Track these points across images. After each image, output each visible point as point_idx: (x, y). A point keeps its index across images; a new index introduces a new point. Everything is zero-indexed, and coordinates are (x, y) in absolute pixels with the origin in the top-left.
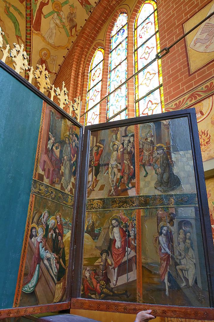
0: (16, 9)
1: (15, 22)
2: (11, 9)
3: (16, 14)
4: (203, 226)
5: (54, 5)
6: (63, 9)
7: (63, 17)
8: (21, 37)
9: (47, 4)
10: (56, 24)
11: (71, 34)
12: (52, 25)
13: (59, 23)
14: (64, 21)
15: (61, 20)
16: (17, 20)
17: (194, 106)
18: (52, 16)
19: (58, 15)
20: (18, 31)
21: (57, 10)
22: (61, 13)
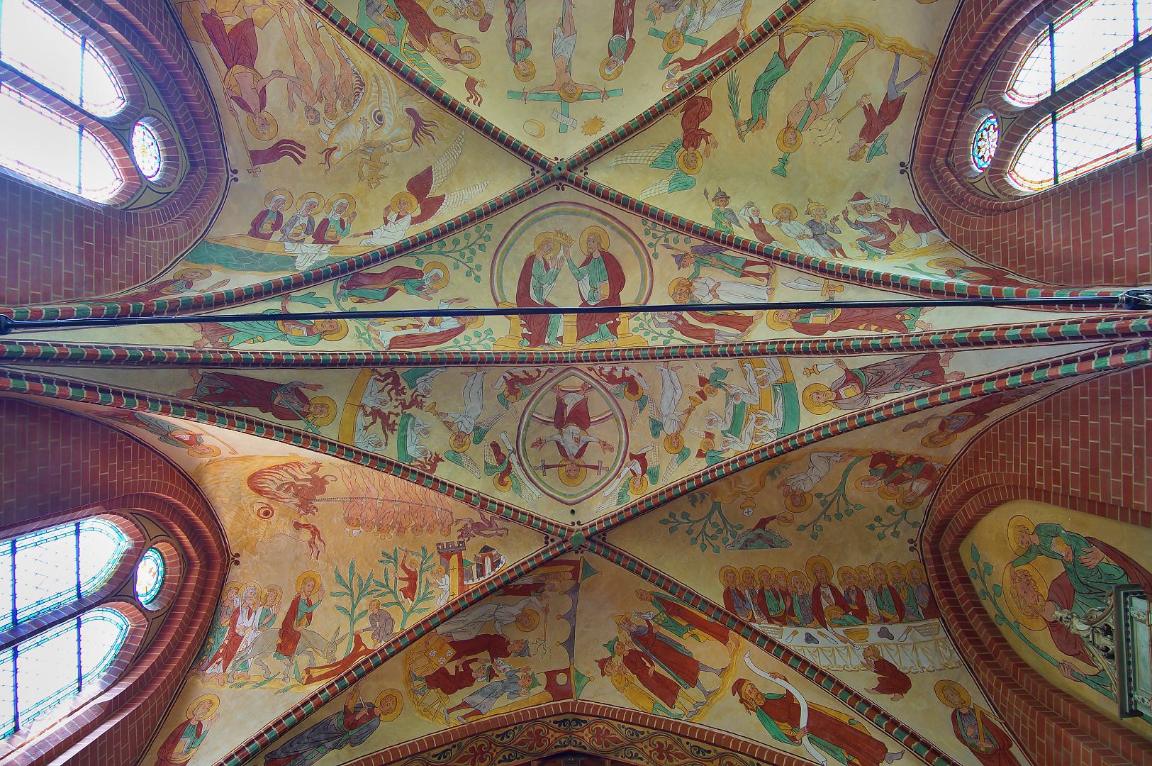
0: (734, 107)
1: (762, 93)
2: (745, 115)
3: (745, 98)
4: (58, 328)
5: (675, 49)
6: (669, 29)
7: (682, 16)
8: (781, 53)
9: (680, 60)
10: (704, 15)
11: (839, 388)
12: (711, 19)
13: (698, 12)
14: (687, 9)
15: (691, 15)
16: (755, 91)
17: (231, 287)
18: (695, 35)
19: (687, 28)
20: (773, 72)
21: (679, 37)
22: (679, 25)
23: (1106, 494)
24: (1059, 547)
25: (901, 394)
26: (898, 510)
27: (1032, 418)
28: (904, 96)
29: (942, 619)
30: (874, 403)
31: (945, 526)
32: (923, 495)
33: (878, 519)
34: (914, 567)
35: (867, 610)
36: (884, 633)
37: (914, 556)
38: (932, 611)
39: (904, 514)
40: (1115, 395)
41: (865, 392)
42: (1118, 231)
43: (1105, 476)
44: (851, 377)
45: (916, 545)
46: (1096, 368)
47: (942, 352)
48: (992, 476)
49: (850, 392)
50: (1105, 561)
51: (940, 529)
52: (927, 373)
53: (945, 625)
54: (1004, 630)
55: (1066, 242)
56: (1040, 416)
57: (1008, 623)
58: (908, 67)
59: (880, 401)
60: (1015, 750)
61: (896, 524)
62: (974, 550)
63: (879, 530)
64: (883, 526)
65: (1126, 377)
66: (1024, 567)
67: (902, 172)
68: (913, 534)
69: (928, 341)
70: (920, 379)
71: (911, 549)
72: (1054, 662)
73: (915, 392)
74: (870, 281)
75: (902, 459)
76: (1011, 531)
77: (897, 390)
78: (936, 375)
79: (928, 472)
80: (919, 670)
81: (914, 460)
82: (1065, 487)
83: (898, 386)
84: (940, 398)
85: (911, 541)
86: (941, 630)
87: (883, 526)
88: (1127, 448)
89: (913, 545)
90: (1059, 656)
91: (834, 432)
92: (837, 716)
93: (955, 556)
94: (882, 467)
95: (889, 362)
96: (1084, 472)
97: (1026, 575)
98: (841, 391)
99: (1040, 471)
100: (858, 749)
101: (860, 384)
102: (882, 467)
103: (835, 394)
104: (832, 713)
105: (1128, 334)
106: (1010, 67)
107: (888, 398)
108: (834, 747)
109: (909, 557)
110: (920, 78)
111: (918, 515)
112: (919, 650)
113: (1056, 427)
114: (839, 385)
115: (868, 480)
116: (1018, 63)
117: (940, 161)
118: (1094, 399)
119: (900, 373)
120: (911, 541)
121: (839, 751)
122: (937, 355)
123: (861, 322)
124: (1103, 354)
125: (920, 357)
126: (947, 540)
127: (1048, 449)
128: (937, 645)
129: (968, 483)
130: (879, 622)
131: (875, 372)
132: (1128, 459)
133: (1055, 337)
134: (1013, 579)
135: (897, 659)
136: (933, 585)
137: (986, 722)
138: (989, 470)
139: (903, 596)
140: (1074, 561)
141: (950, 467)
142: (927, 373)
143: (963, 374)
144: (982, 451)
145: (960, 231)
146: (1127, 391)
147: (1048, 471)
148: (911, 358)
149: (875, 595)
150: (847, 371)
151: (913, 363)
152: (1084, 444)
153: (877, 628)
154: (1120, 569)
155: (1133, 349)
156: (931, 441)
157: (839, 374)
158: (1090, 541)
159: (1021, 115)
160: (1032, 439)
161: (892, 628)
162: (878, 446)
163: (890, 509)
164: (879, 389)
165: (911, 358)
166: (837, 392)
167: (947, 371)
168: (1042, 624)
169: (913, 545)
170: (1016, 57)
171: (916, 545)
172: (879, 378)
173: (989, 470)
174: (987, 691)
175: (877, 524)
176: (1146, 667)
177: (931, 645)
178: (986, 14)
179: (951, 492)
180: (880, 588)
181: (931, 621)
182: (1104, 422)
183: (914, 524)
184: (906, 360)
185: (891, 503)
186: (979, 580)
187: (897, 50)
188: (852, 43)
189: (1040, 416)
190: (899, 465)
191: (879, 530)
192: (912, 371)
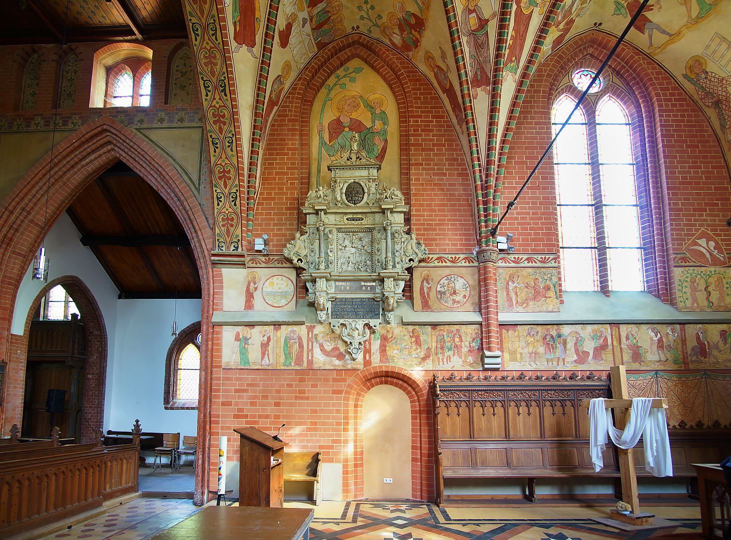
11: (476, 13)
23: (414, 155)
24: (378, 125)
25: (468, 60)
26: (379, 22)
27: (443, 117)
28: (643, 33)
29: (318, 53)
30: (464, 39)
31: (371, 51)
32: (391, 40)
33: (372, 8)
34: (343, 31)
35: (315, 6)
36: (305, 21)
37: (349, 30)
38: (321, 46)
39: (376, 25)
40: (457, 160)
41: (472, 34)
42: (525, 163)
43: (422, 155)
44: (483, 23)
45: (356, 30)
46: (474, 164)
47: (490, 88)
48: (409, 92)
49: (473, 20)
50: (379, 148)
51: (368, 48)
52: (479, 77)
53: (315, 55)
54: (323, 90)
55: (526, 138)
56: (444, 122)
57: (328, 94)
58: (659, 38)
59: (465, 44)
60: (276, 108)
61: (370, 19)
62: (358, 70)
63: (365, 7)
64: (368, 11)
65: (464, 165)
66: (362, 104)
67: (595, 24)
68: (363, 29)
69: (498, 84)
70: (476, 73)
71: (353, 28)
72: (321, 121)
73: (469, 68)
74: (540, 37)
75: (416, 34)
76: (378, 96)
77: (471, 57)
78: (477, 83)
79: (406, 47)
80: (292, 49)
81: (416, 43)
82: (413, 135)
83: (473, 57)
84: (465, 87)
85: (358, 27)
86: (312, 54)
87: (368, 11)
88: (435, 165)
89: (356, 28)
90: (326, 124)
91: (448, 10)
92: (257, 8)
93: (353, 56)
94: (413, 21)
95: (488, 52)
96: (421, 145)
97: (358, 106)
98: (474, 15)
99: (417, 121)
100: (245, 28)
101: (477, 30)
102: (413, 21)
103: (472, 9)
104: (257, 5)
105: (487, 176)
106: (622, 100)
107: (466, 50)
108: (238, 9)
109: (348, 26)
110: (648, 42)
111: (376, 34)
112: (300, 45)
113: (440, 131)
114: (478, 13)
115: (402, 8)
116: (624, 108)
117: (591, 50)
118: (456, 150)
119: (481, 59)
120: (358, 27)
121: (237, 14)
122: (488, 85)
123: (516, 33)
124: (480, 165)
125: (489, 74)
126: (363, 52)
127: (429, 126)
128: (305, 54)
129: (402, 74)
130: (310, 16)
131: (484, 42)
132: (430, 165)
133: (490, 149)
134: (353, 97)
135: (294, 34)
136: (334, 44)
137: (281, 91)
138: (413, 89)
139: (326, 27)
140: (374, 132)
141: (410, 61)
142: (479, 77)
143: (476, 99)
144: (422, 84)
145: (546, 71)
146: (458, 165)
147: (418, 126)
148: (489, 68)
149: (324, 9)
150: (487, 21)
151: (486, 69)
152: (434, 145)
153: (307, 17)
154: (377, 155)
155: (481, 177)
156: (429, 58)
157: (486, 14)
158: (386, 141)
159: (594, 108)
160: (433, 117)
161: (308, 25)
162: (429, 25)
163: (380, 17)
164: (472, 44)
165: (489, 68)
166: (474, 11)
167: (479, 90)
168: (338, 115)
169: (356, 28)
170: (625, 103)
171: (356, 30)
172: (479, 46)
173: (413, 89)
174: (293, 88)
175: (369, 6)
176: (351, 174)
177: (304, 51)
178: (657, 95)
179: (392, 57)
180: (328, 12)
181: (315, 47)
182: (444, 155)
183: (369, 31)
184: (488, 65)
185: (385, 19)
186: (344, 73)
187: (674, 37)
188: (701, 9)
189: (444, 122)
190: (414, 32)
191: (365, 7)
192: (481, 68)
